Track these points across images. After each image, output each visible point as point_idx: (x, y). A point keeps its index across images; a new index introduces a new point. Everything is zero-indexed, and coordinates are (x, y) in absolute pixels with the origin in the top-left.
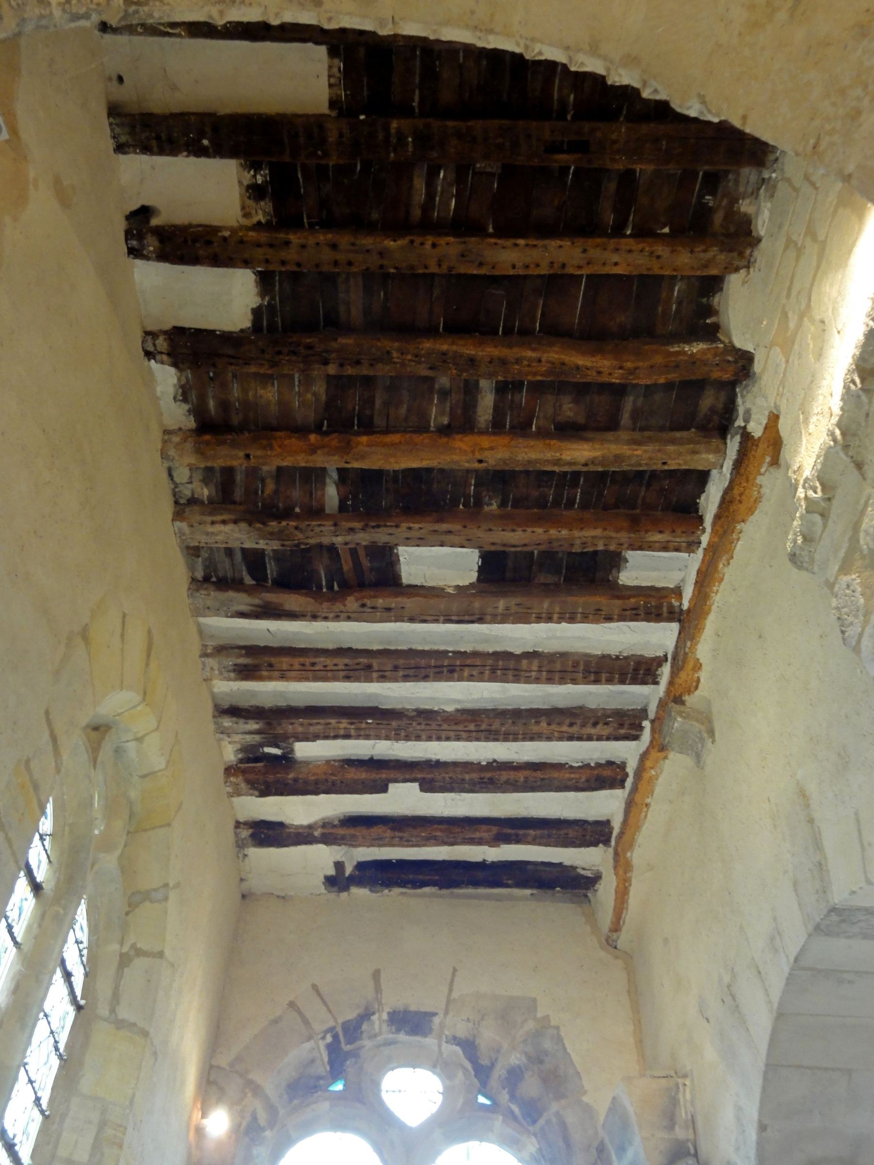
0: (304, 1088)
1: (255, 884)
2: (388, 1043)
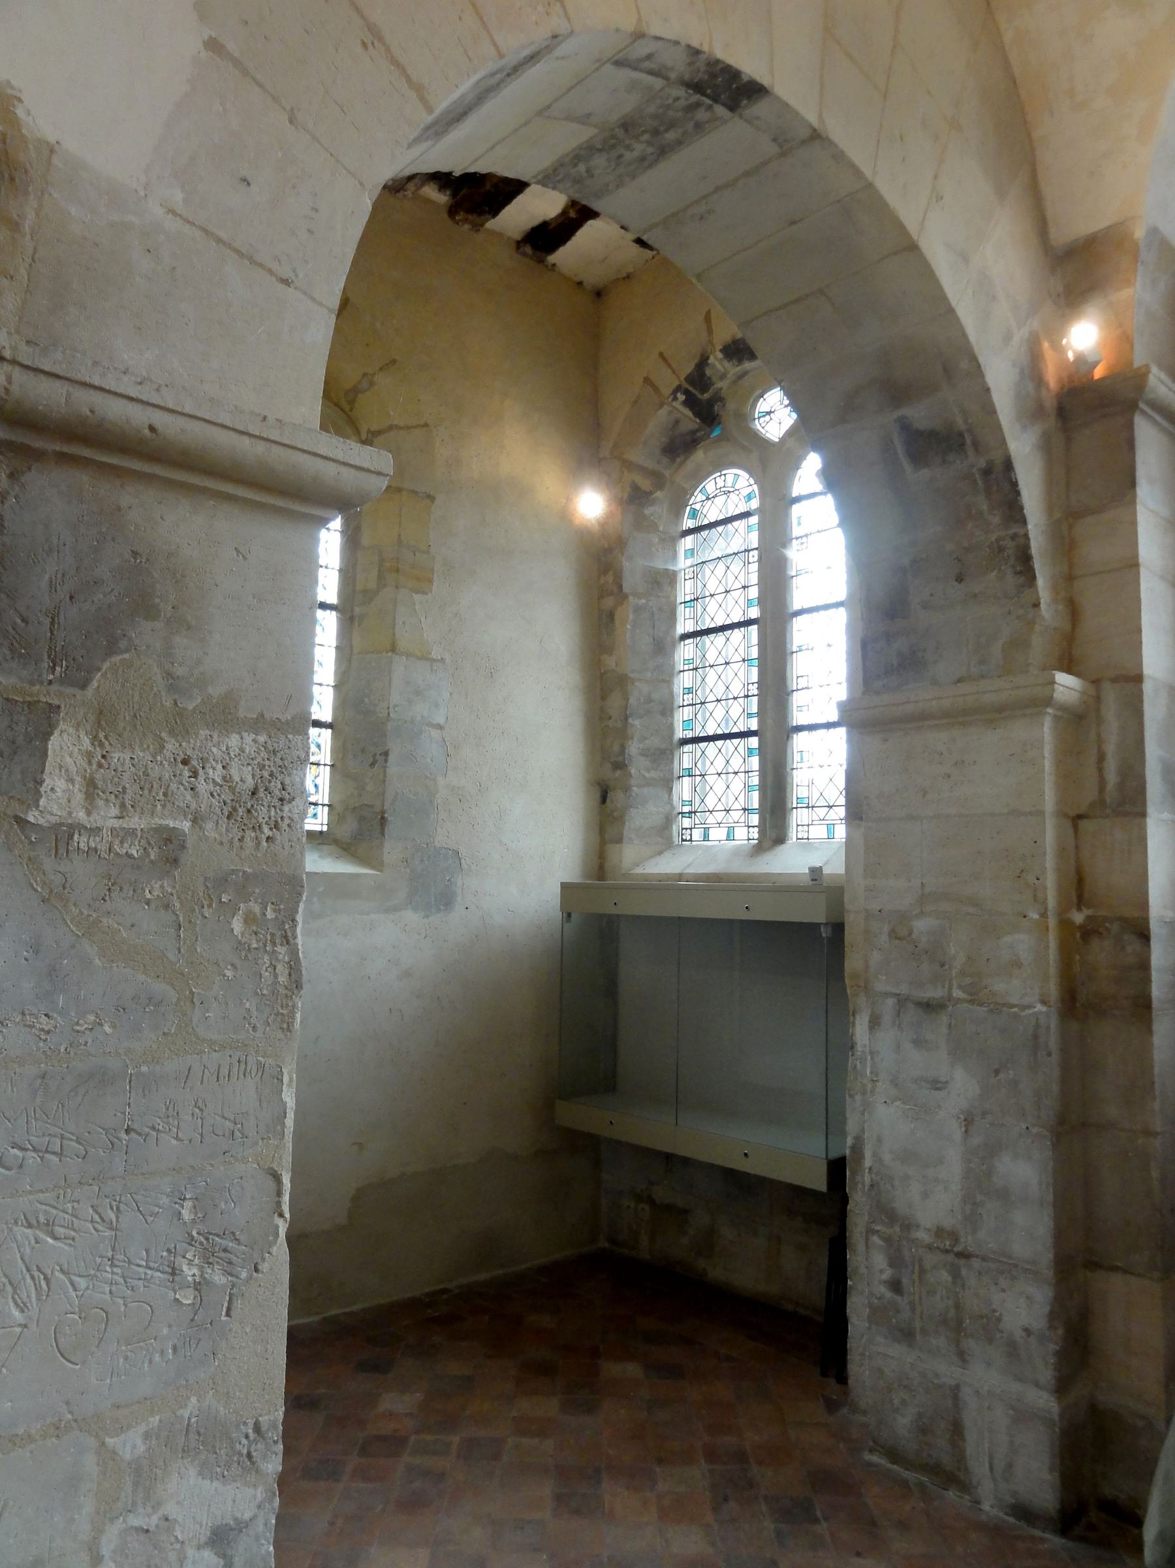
0: (679, 447)
1: (594, 277)
2: (741, 376)
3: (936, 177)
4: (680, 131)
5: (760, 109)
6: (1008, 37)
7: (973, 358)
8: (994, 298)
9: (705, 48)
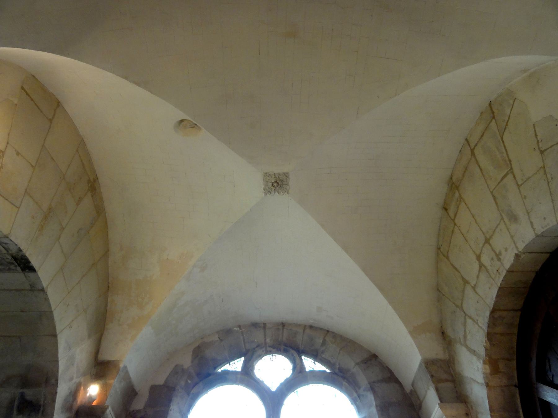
3: (73, 321)
4: (3, 267)
5: (31, 275)
6: (109, 299)
7: (57, 380)
8: (73, 365)
9: (24, 251)
